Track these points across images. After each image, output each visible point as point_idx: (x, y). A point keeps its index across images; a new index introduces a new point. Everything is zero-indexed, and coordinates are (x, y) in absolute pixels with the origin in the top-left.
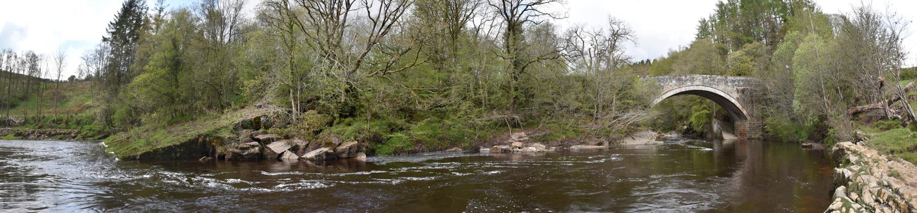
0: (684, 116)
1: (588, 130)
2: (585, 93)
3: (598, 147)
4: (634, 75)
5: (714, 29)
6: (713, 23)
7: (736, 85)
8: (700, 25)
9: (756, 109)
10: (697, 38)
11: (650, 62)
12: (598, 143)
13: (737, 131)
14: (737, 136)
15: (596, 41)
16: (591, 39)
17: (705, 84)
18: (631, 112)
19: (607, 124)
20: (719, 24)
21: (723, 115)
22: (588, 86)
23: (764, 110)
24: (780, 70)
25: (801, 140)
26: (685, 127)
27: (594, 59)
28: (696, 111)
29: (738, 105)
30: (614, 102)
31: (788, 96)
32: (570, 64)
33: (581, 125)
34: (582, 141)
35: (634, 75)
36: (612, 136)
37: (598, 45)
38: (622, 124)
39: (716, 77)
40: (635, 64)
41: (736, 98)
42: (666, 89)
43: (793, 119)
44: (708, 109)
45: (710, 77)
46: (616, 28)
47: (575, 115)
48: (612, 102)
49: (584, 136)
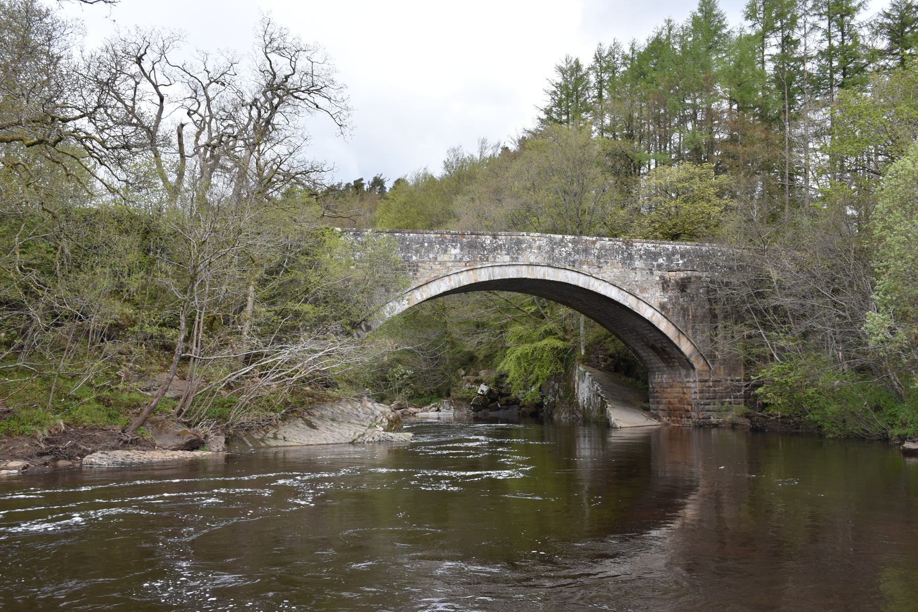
0: (481, 355)
1: (151, 399)
2: (148, 272)
3: (189, 455)
4: (323, 226)
5: (605, 94)
6: (606, 77)
7: (659, 267)
8: (559, 80)
9: (725, 338)
10: (542, 121)
11: (383, 188)
12: (186, 440)
13: (658, 403)
14: (656, 417)
15: (209, 101)
16: (190, 93)
17: (558, 260)
18: (305, 343)
19: (222, 377)
20: (624, 80)
21: (611, 356)
22: (163, 250)
23: (756, 342)
24: (820, 222)
25: (896, 432)
26: (483, 388)
27: (193, 163)
28: (520, 339)
29: (663, 325)
30: (249, 308)
31: (848, 299)
32: (101, 172)
33: (128, 380)
34: (128, 436)
35: (323, 226)
36: (238, 417)
37: (212, 117)
38: (271, 378)
39: (594, 243)
40: (332, 189)
41: (656, 306)
42: (424, 274)
43: (861, 369)
44: (561, 334)
45: (573, 242)
46: (282, 66)
47: (108, 345)
48: (241, 309)
49: (138, 420)
